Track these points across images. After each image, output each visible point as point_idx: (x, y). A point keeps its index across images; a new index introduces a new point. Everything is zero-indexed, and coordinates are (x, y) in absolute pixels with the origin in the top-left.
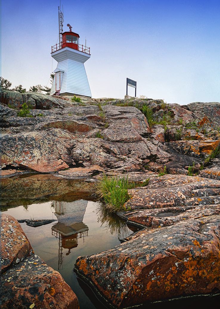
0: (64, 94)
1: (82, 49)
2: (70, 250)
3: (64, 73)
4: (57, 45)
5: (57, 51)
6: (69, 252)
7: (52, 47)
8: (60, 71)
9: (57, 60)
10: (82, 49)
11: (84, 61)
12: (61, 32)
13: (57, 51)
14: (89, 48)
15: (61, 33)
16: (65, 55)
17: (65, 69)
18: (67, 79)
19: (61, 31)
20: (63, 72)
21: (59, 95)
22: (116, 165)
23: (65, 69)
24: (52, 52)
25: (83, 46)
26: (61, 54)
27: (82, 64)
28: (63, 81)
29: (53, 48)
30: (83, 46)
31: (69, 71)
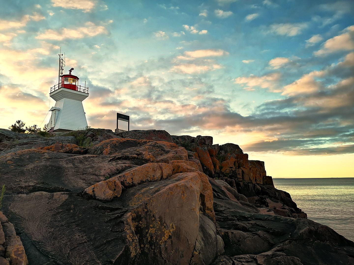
0: (57, 130)
1: (80, 89)
2: (70, 73)
3: (60, 111)
4: (55, 86)
5: (55, 91)
6: (70, 71)
7: (51, 88)
8: (55, 109)
9: (54, 98)
10: (80, 89)
11: (82, 99)
12: (61, 75)
13: (55, 91)
14: (88, 88)
15: (60, 76)
16: (62, 94)
17: (59, 106)
18: (62, 113)
19: (61, 74)
20: (59, 110)
21: (53, 132)
22: (169, 251)
23: (59, 106)
24: (51, 93)
25: (80, 86)
26: (57, 95)
27: (80, 102)
28: (57, 121)
29: (52, 89)
30: (80, 86)
31: (64, 112)
